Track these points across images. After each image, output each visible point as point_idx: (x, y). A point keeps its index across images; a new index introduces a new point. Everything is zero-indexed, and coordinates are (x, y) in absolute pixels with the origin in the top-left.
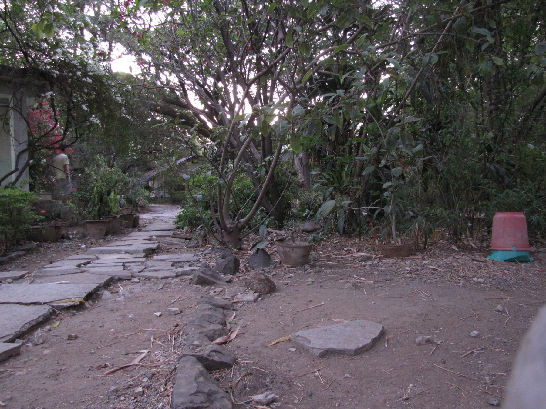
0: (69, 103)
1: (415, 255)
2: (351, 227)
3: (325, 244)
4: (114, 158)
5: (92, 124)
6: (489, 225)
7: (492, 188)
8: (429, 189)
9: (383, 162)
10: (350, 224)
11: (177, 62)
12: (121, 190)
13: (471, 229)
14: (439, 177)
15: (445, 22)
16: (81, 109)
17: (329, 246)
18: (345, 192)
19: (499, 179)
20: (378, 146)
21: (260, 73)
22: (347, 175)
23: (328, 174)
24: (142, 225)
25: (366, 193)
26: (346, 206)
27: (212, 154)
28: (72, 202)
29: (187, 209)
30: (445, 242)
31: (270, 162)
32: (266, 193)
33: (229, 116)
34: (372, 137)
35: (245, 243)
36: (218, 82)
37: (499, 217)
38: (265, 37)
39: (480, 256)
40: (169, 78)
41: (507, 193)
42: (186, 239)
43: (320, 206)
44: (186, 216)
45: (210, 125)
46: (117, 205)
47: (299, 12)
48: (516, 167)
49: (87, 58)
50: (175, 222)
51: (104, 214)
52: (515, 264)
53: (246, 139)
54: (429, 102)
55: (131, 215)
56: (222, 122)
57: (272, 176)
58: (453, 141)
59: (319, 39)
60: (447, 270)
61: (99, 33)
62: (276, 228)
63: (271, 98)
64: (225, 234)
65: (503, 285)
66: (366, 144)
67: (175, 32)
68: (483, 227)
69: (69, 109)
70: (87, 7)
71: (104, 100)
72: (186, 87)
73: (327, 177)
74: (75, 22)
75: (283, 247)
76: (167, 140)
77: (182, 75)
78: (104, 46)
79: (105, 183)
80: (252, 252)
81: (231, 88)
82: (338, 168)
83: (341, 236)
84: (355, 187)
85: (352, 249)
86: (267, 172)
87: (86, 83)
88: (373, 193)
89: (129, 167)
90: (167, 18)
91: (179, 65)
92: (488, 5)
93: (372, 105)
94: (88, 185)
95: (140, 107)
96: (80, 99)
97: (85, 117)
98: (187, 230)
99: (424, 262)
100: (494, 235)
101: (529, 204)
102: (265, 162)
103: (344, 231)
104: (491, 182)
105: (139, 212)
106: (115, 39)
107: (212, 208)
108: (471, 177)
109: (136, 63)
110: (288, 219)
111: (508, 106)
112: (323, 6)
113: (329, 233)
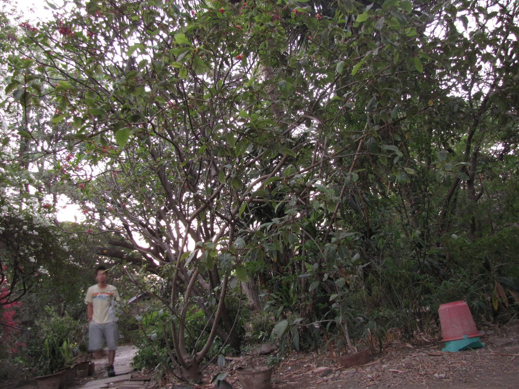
0: (16, 257)
1: (373, 360)
2: (307, 342)
3: (284, 365)
4: (65, 306)
5: (40, 275)
6: (436, 316)
7: (431, 282)
9: (326, 276)
10: (305, 340)
11: (119, 206)
12: (74, 338)
13: (421, 324)
14: (380, 280)
16: (29, 261)
17: (289, 366)
18: (296, 310)
19: (435, 271)
20: (318, 260)
21: (199, 209)
22: (294, 293)
23: (277, 295)
24: (98, 372)
25: (315, 308)
26: (298, 323)
28: (21, 359)
29: (143, 348)
30: (399, 342)
31: (219, 291)
32: (220, 322)
33: (173, 252)
34: (312, 254)
35: (205, 375)
37: (443, 308)
38: (199, 174)
39: (435, 349)
40: (113, 222)
41: (445, 284)
42: (145, 381)
43: (273, 326)
44: (142, 356)
45: (157, 262)
46: (71, 355)
47: (227, 151)
48: (447, 257)
49: (33, 212)
50: (132, 364)
51: (56, 367)
52: (469, 352)
53: (193, 272)
54: (357, 212)
55: (86, 363)
56: (168, 259)
57: (223, 304)
58: (386, 244)
59: (249, 170)
60: (407, 370)
61: (44, 187)
62: (233, 356)
63: (212, 228)
64: (184, 369)
65: (465, 377)
66: (307, 261)
68: (431, 319)
69: (16, 264)
70: (31, 164)
71: (51, 250)
72: (130, 229)
73: (276, 297)
74: (20, 180)
75: (243, 375)
77: (125, 218)
78: (48, 199)
79: (56, 334)
80: (213, 385)
81: (173, 225)
82: (284, 287)
83: (299, 353)
84: (304, 303)
85: (311, 365)
86: (217, 302)
87: (32, 235)
88: (322, 306)
89: (80, 313)
90: (106, 167)
91: (122, 208)
92: (390, 123)
93: (306, 224)
94: (39, 338)
95: (86, 252)
96: (27, 251)
97: (33, 269)
98: (145, 371)
99: (384, 366)
100: (443, 326)
101: (466, 291)
102: (214, 292)
103: (301, 347)
104: (428, 276)
105: (94, 358)
106: (59, 190)
107: (168, 345)
109: (81, 211)
110: (244, 344)
111: (427, 204)
112: (248, 144)
113: (287, 352)
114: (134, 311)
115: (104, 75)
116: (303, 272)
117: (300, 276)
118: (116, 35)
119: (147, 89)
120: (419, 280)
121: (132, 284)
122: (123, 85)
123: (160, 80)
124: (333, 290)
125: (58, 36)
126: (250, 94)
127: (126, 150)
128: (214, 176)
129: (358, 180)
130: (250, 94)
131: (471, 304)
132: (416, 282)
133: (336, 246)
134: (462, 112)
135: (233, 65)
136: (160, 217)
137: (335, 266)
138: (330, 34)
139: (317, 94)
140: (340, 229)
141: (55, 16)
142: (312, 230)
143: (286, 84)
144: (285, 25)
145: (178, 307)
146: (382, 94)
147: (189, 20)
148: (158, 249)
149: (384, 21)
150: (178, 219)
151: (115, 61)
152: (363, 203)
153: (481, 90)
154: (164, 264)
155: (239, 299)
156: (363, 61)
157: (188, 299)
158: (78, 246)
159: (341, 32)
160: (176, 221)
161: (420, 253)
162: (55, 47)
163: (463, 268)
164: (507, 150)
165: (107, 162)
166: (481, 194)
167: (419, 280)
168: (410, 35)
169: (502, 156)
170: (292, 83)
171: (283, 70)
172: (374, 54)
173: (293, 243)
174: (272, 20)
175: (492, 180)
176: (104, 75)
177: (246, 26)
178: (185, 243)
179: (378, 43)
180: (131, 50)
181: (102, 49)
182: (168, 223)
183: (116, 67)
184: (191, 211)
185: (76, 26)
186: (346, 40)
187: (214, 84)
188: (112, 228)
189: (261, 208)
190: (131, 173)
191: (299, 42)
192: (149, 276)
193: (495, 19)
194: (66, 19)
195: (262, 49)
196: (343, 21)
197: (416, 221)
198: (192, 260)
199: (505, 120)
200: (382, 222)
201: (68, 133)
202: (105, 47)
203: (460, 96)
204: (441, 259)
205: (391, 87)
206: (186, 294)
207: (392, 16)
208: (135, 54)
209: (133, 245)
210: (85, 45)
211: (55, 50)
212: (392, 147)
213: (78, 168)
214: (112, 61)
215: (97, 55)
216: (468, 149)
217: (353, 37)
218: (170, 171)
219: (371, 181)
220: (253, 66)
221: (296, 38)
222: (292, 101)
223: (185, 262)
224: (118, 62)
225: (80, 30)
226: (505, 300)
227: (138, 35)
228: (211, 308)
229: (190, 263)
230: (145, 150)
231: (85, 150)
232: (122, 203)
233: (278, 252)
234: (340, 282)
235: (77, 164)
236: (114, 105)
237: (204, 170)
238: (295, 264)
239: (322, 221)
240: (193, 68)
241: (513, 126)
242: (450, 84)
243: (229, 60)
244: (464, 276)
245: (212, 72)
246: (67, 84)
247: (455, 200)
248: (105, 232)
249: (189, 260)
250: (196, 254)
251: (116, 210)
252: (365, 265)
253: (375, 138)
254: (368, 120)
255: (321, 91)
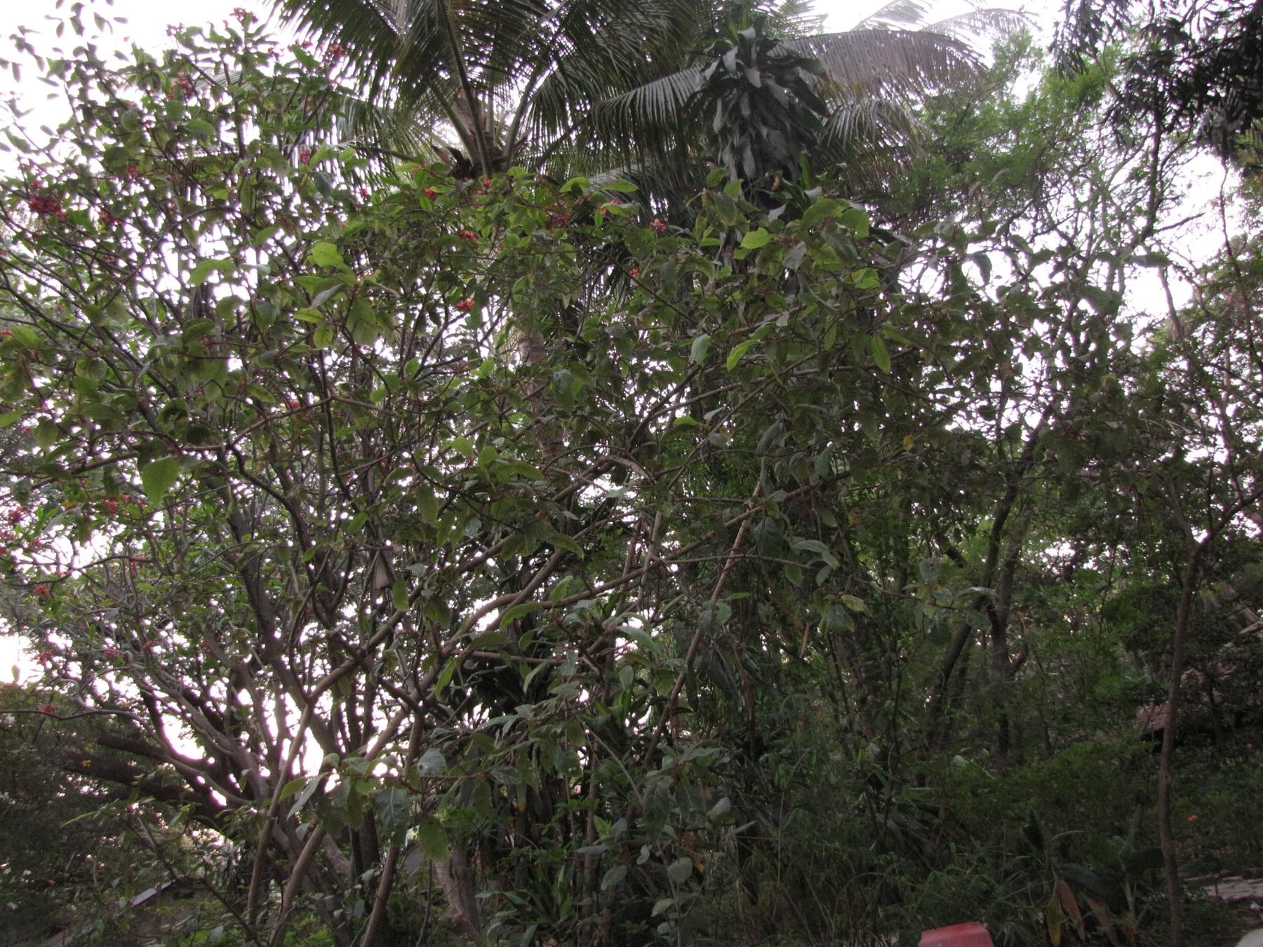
7: (901, 873)
8: (761, 898)
9: (645, 851)
11: (135, 646)
14: (779, 864)
15: (730, 527)
19: (911, 847)
20: (629, 812)
23: (523, 896)
27: (227, 869)
31: (374, 882)
33: (265, 772)
34: (613, 794)
36: (239, 690)
38: (346, 580)
40: (116, 686)
45: (221, 799)
48: (942, 813)
53: (311, 830)
54: (728, 696)
56: (250, 792)
57: (383, 917)
59: (469, 577)
63: (368, 717)
66: (600, 812)
67: (133, 577)
73: (518, 900)
76: (108, 843)
81: (269, 705)
82: (541, 877)
86: (368, 908)
90: (113, 546)
91: (142, 654)
93: (601, 718)
95: (34, 765)
101: (987, 896)
102: (362, 882)
104: (895, 857)
108: (851, 856)
109: (36, 653)
112: (469, 518)
114: (146, 929)
115: (131, 320)
116: (589, 838)
117: (581, 850)
118: (170, 226)
119: (235, 364)
120: (872, 869)
121: (150, 852)
122: (173, 351)
123: (267, 348)
124: (663, 886)
125: (25, 217)
126: (484, 396)
127: (169, 508)
128: (383, 589)
129: (732, 617)
130: (484, 396)
131: (997, 930)
132: (867, 874)
133: (670, 780)
134: (978, 467)
135: (447, 323)
136: (237, 683)
137: (668, 829)
138: (682, 269)
139: (643, 408)
140: (687, 733)
141: (24, 168)
142: (613, 737)
143: (570, 380)
144: (578, 238)
145: (264, 921)
146: (797, 416)
147: (352, 208)
148: (226, 764)
149: (804, 251)
150: (284, 691)
151: (160, 288)
152: (743, 673)
153: (1022, 416)
154: (238, 805)
155: (426, 904)
156: (755, 338)
157: (291, 899)
158: (13, 746)
159: (707, 266)
160: (278, 693)
161: (877, 798)
162: (15, 242)
163: (978, 838)
164: (1081, 556)
165: (114, 533)
166: (1022, 661)
167: (872, 869)
168: (863, 287)
169: (1071, 571)
170: (584, 377)
171: (568, 344)
172: (778, 324)
173: (565, 768)
174: (549, 226)
175: (1047, 627)
176: (131, 320)
177: (486, 232)
178: (297, 751)
179: (790, 298)
180: (205, 265)
181: (134, 257)
182: (258, 698)
183: (163, 302)
184: (318, 672)
185: (73, 197)
186: (717, 285)
187: (400, 364)
188: (111, 703)
189: (494, 674)
190: (176, 566)
191: (609, 280)
192: (196, 833)
193: (1048, 267)
194: (49, 178)
195: (520, 292)
196: (713, 241)
197: (869, 718)
198: (313, 797)
199: (1074, 491)
200: (787, 721)
201: (22, 453)
202: (140, 255)
203: (976, 427)
204: (928, 816)
205: (816, 401)
206: (289, 886)
207: (823, 241)
208: (214, 278)
209: (160, 751)
210: (90, 244)
211: (13, 248)
212: (815, 545)
213: (37, 543)
214: (154, 288)
215: (119, 271)
216: (994, 553)
217: (735, 279)
218: (273, 570)
219: (765, 621)
220: (498, 328)
221: (604, 271)
222: (584, 420)
223: (293, 801)
224: (168, 292)
225: (83, 207)
226: (1077, 920)
227: (226, 231)
228: (352, 923)
229: (306, 806)
230: (217, 512)
231: (62, 501)
232: (144, 640)
233: (529, 791)
234: (679, 869)
235: (37, 533)
236: (149, 396)
237: (360, 570)
238: (570, 818)
239: (644, 713)
240: (349, 326)
241: (1093, 504)
242: (954, 400)
243: (440, 310)
244: (981, 860)
245: (397, 335)
246: (31, 334)
247: (963, 671)
248: (92, 714)
249: (303, 797)
250: (323, 782)
251: (126, 658)
252: (743, 828)
253: (777, 521)
254: (762, 475)
255: (653, 400)
